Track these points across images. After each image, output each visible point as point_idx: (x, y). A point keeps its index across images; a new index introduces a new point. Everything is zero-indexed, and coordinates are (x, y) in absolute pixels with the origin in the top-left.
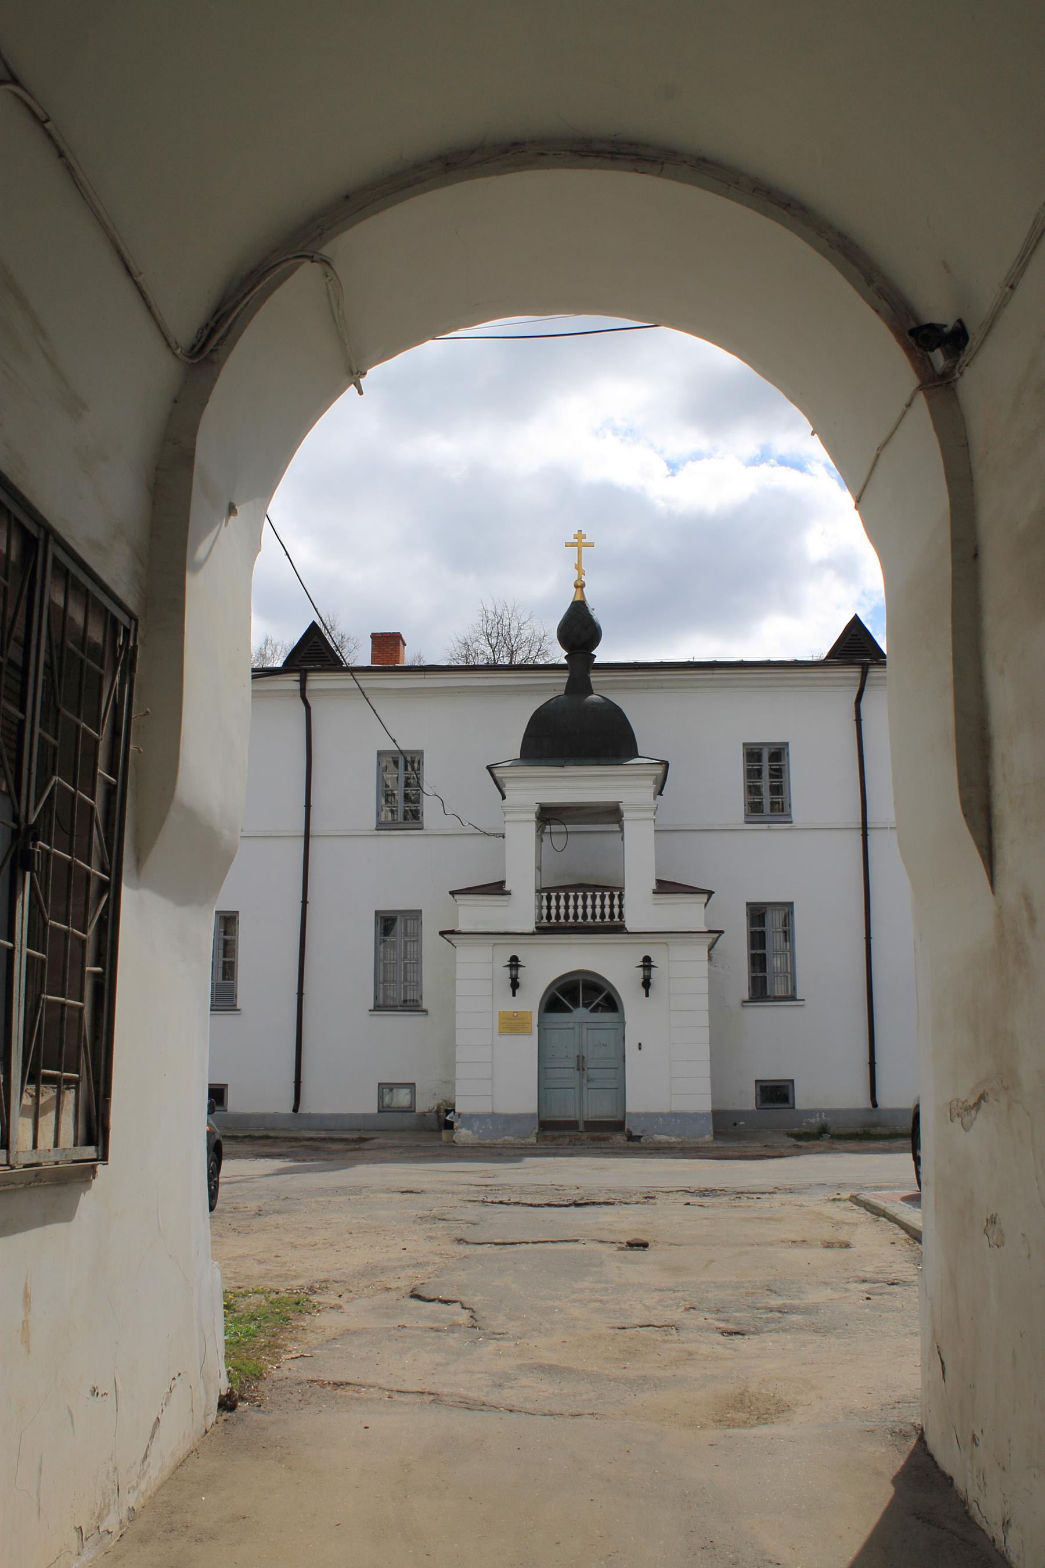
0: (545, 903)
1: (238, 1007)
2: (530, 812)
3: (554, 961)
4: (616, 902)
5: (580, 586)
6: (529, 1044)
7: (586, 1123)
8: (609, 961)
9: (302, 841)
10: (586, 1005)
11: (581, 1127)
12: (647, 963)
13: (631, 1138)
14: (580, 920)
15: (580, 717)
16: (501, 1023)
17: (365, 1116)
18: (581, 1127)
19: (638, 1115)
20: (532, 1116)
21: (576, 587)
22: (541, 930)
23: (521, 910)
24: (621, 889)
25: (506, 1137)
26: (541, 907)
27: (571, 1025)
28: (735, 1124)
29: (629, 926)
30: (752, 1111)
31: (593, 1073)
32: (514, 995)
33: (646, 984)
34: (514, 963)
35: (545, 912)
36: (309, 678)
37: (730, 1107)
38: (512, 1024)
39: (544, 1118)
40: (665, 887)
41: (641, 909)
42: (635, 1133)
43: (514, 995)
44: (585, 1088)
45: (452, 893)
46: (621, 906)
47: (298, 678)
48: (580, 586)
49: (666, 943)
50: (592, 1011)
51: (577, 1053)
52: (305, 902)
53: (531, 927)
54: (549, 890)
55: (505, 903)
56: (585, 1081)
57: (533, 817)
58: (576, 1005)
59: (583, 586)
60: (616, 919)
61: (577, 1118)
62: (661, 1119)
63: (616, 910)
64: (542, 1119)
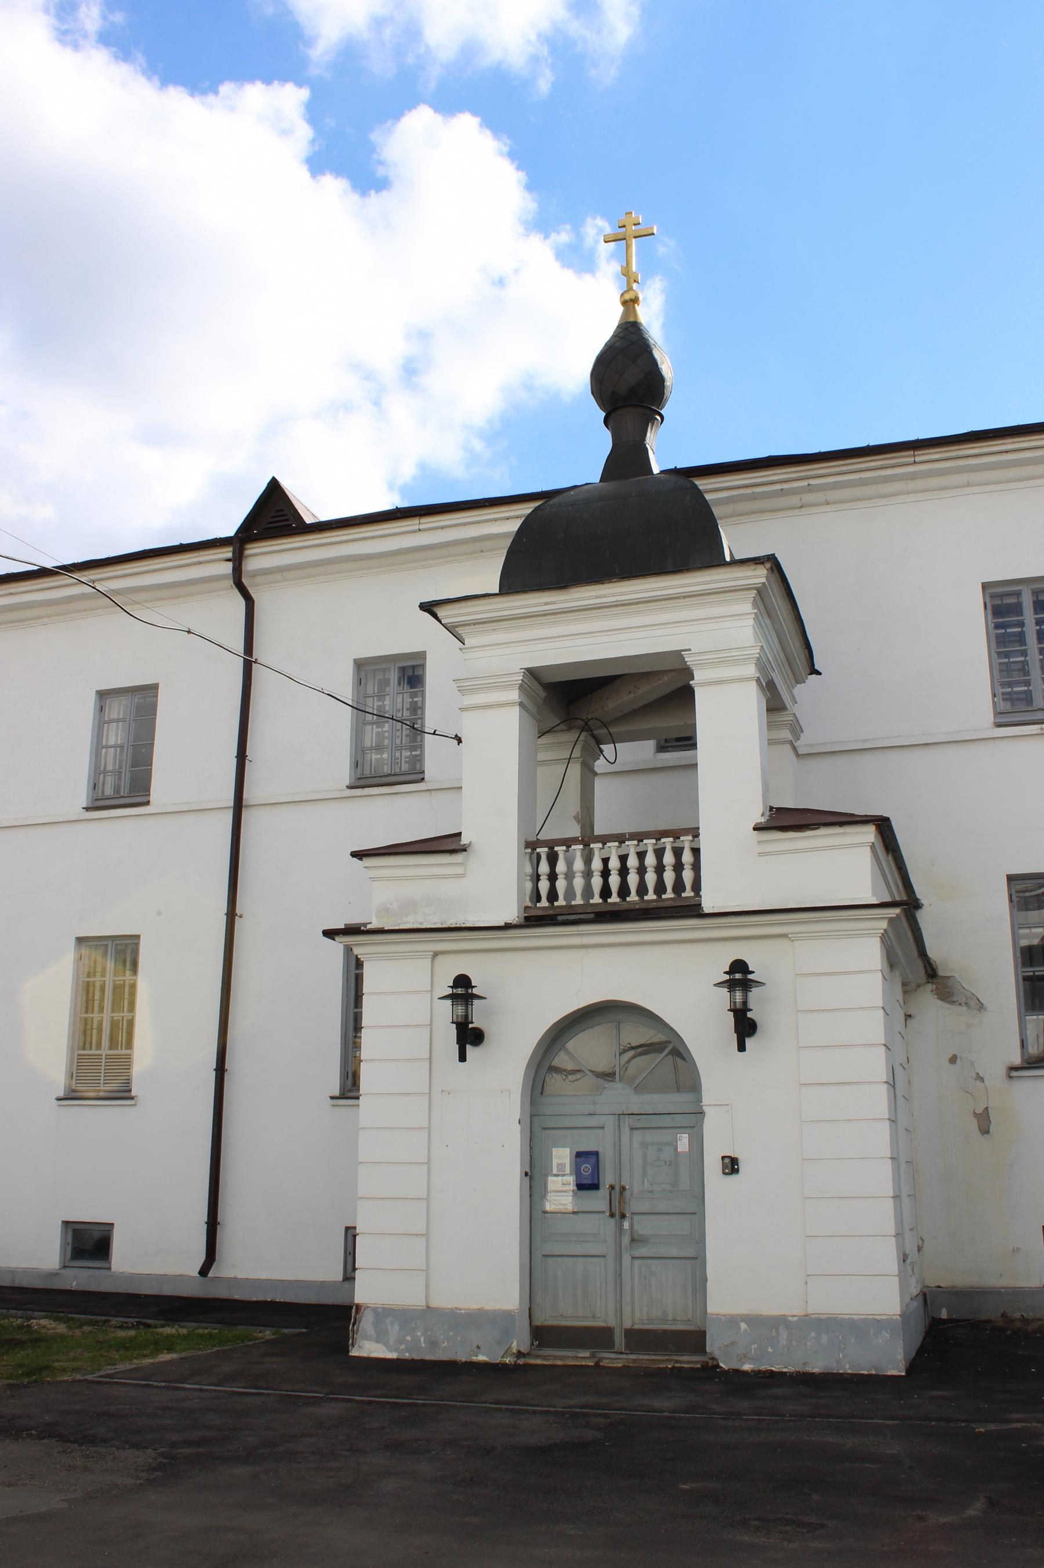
0: (544, 868)
1: (133, 1093)
3: (541, 985)
4: (687, 857)
7: (630, 1333)
8: (669, 978)
11: (619, 1341)
12: (739, 977)
14: (614, 899)
15: (623, 518)
17: (321, 1285)
18: (619, 1341)
19: (733, 1321)
21: (624, 303)
22: (534, 920)
23: (491, 884)
24: (695, 833)
26: (537, 878)
29: (708, 905)
31: (644, 1226)
32: (742, 1047)
33: (745, 1027)
34: (463, 990)
35: (544, 886)
36: (247, 552)
39: (545, 1317)
40: (784, 821)
41: (736, 867)
43: (742, 1047)
44: (626, 1259)
45: (358, 855)
46: (696, 867)
47: (230, 555)
48: (630, 303)
49: (785, 936)
52: (845, 973)
53: (511, 913)
55: (459, 870)
56: (626, 1240)
57: (514, 695)
59: (635, 301)
60: (688, 893)
61: (611, 1323)
62: (784, 1334)
63: (688, 875)
64: (538, 1321)
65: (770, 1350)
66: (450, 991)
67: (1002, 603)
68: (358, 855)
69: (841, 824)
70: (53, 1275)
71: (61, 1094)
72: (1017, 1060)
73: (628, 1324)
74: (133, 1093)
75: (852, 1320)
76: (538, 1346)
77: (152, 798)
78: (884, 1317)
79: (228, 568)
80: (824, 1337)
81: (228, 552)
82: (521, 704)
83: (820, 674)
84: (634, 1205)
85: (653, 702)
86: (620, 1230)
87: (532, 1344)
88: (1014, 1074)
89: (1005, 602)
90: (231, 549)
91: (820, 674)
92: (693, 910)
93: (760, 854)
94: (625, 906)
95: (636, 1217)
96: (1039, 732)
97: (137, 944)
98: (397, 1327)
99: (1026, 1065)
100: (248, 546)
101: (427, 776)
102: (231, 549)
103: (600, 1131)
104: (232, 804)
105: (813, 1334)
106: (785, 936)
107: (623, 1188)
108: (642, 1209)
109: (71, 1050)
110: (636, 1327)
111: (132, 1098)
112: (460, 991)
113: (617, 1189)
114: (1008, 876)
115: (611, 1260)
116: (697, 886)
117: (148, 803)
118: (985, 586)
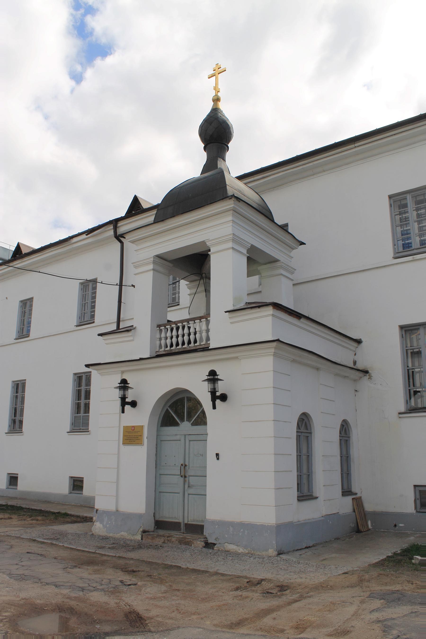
2: (148, 264)
3: (155, 384)
5: (216, 100)
6: (140, 454)
9: (124, 283)
10: (189, 419)
13: (208, 545)
16: (124, 436)
20: (140, 516)
23: (141, 344)
25: (122, 533)
27: (178, 437)
28: (395, 526)
30: (412, 514)
34: (124, 385)
36: (119, 225)
37: (391, 509)
38: (131, 436)
41: (222, 330)
42: (210, 541)
48: (216, 100)
49: (237, 358)
50: (192, 424)
51: (182, 462)
54: (159, 326)
55: (131, 338)
56: (186, 486)
58: (182, 420)
61: (181, 520)
62: (231, 529)
65: (226, 536)
66: (118, 385)
67: (398, 201)
68: (99, 335)
69: (259, 307)
70: (65, 496)
71: (69, 431)
72: (403, 410)
73: (186, 522)
74: (89, 430)
75: (256, 525)
76: (157, 528)
77: (95, 321)
78: (270, 524)
79: (112, 233)
80: (246, 531)
81: (111, 227)
82: (153, 270)
83: (305, 244)
84: (190, 472)
85: (196, 264)
86: (185, 481)
87: (155, 527)
88: (401, 416)
89: (402, 203)
90: (112, 225)
91: (305, 244)
92: (206, 349)
93: (232, 323)
94: (189, 349)
95: (191, 477)
96: (412, 259)
97: (90, 375)
98: (106, 518)
99: (408, 411)
100: (119, 222)
101: (180, 303)
102: (112, 225)
103: (179, 442)
104: (116, 321)
105: (242, 530)
106: (237, 358)
107: (186, 465)
108: (192, 474)
109: (72, 414)
110: (189, 523)
111: (88, 431)
112: (122, 385)
113: (184, 466)
114: (400, 326)
115: (181, 494)
116: (208, 339)
117: (94, 322)
118: (390, 197)
